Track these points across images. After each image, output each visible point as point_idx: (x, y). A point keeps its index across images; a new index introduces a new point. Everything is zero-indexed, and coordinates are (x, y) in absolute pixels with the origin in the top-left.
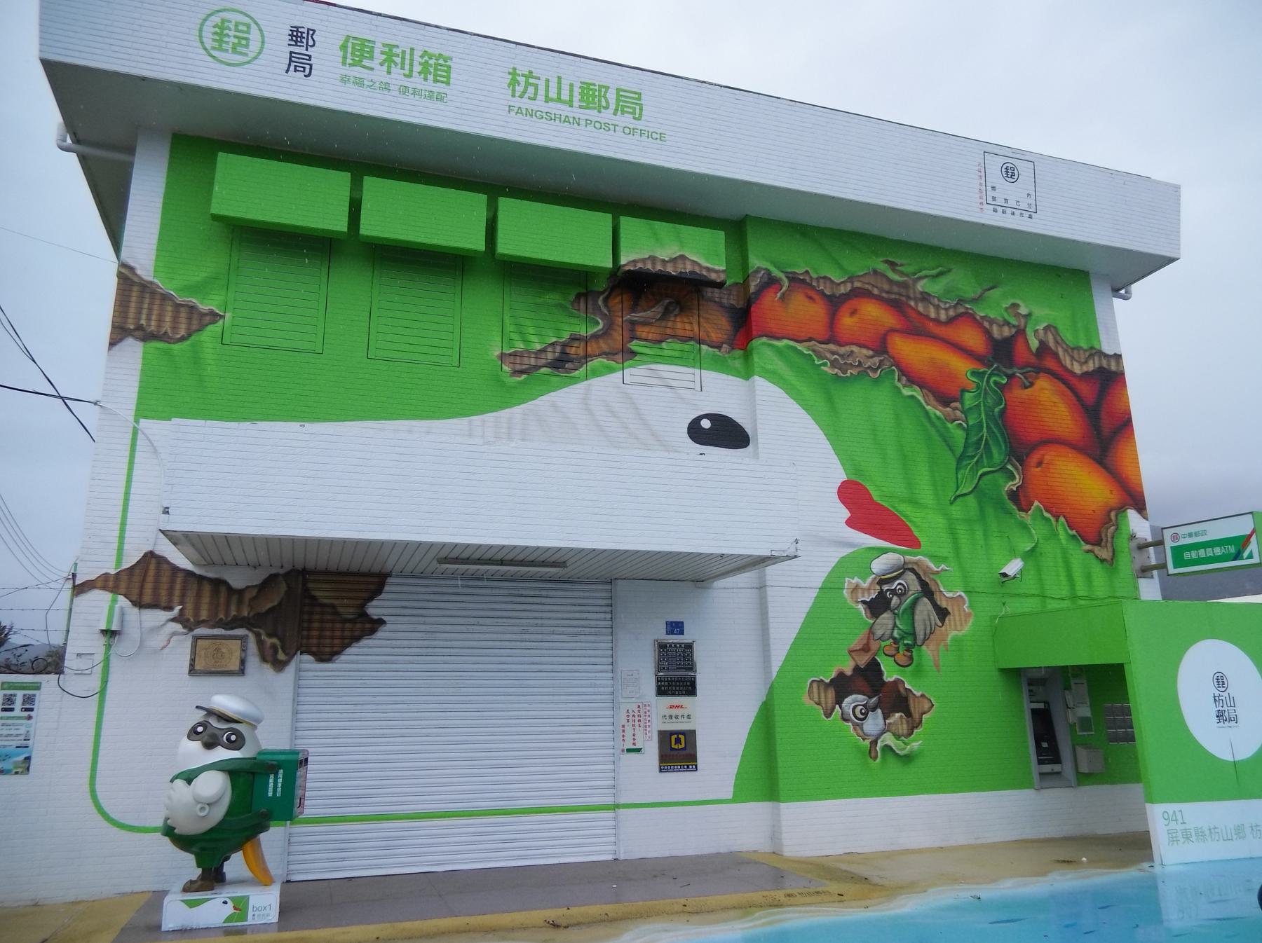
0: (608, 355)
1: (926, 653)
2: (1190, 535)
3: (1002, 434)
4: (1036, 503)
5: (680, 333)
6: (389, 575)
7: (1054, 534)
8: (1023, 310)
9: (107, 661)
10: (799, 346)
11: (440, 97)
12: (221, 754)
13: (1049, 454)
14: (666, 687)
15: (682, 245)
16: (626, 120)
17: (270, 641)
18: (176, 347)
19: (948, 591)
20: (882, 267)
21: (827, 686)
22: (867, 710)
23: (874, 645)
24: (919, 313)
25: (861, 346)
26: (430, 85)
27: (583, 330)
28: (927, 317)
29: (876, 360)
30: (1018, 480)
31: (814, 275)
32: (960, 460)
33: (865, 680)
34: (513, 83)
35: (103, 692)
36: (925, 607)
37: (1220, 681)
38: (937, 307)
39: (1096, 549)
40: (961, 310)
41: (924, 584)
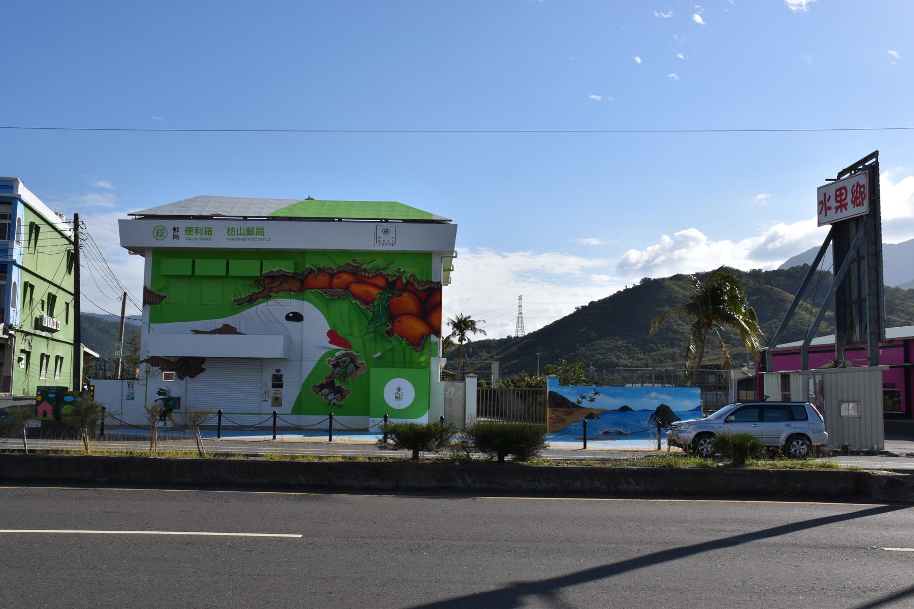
1: (350, 379)
14: (274, 386)
20: (350, 262)
22: (329, 393)
26: (208, 237)
27: (256, 291)
33: (329, 385)
37: (399, 389)
41: (352, 359)
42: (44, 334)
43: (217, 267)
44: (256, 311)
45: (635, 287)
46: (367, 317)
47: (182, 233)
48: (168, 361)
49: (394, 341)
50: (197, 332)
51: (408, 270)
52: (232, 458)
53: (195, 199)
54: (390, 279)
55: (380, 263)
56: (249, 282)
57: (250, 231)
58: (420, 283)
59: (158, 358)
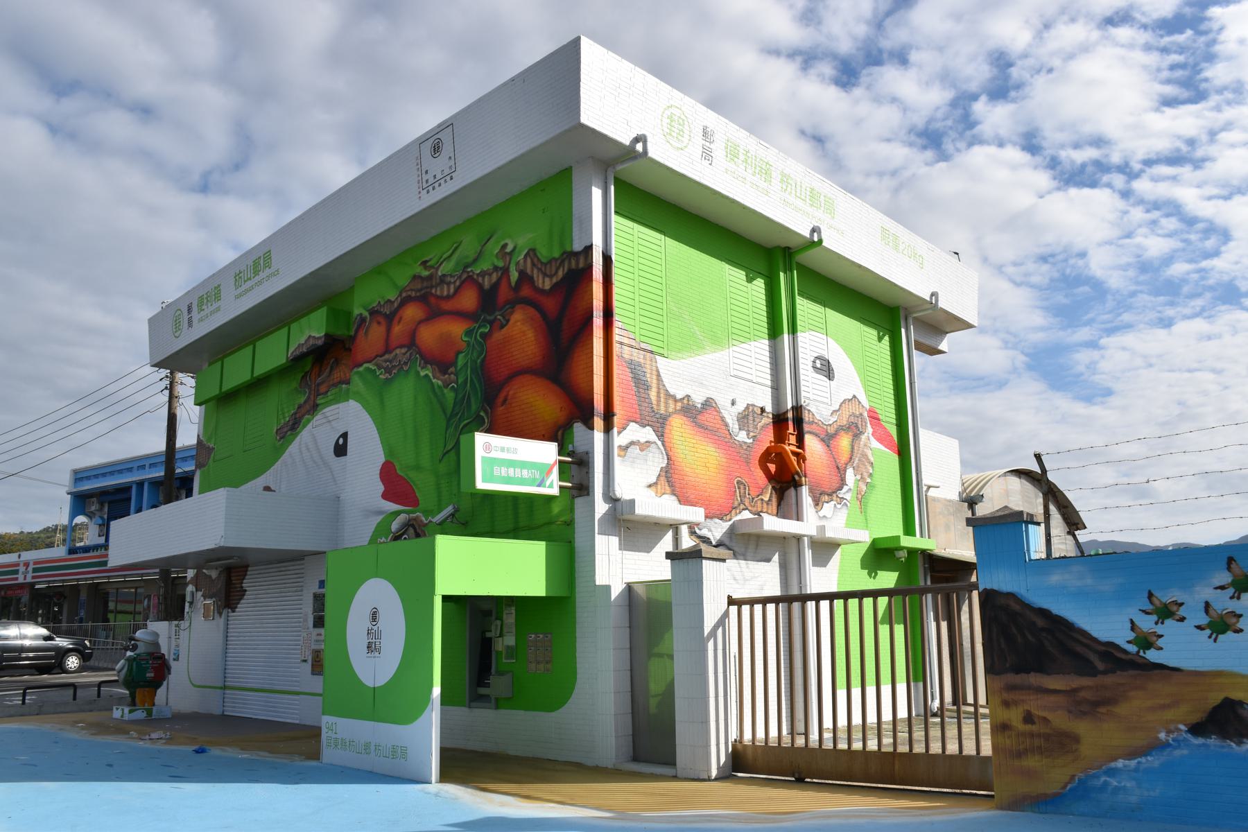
0: (308, 412)
2: (503, 449)
6: (247, 566)
32: (449, 420)
42: (31, 655)
58: (545, 267)
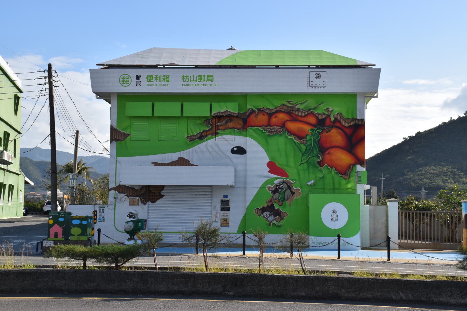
0: (212, 134)
1: (287, 203)
3: (318, 146)
4: (326, 164)
5: (230, 127)
7: (331, 172)
8: (330, 109)
9: (115, 203)
10: (259, 128)
11: (167, 85)
12: (132, 219)
13: (332, 151)
14: (222, 209)
15: (227, 108)
16: (210, 82)
17: (143, 199)
18: (122, 142)
19: (295, 188)
20: (285, 103)
21: (260, 210)
22: (270, 215)
23: (273, 201)
24: (296, 115)
25: (277, 126)
26: (165, 83)
27: (206, 129)
28: (298, 116)
29: (281, 129)
30: (321, 158)
31: (265, 108)
32: (303, 155)
33: (270, 208)
34: (183, 78)
35: (115, 208)
36: (288, 192)
37: (334, 212)
38: (302, 112)
39: (344, 176)
40: (309, 112)
43: (172, 109)
44: (206, 146)
45: (460, 119)
46: (301, 151)
47: (143, 80)
48: (133, 189)
49: (325, 170)
50: (157, 164)
51: (335, 109)
52: (323, 275)
53: (150, 51)
54: (320, 117)
55: (311, 103)
56: (199, 122)
57: (201, 78)
58: (346, 120)
59: (124, 186)
